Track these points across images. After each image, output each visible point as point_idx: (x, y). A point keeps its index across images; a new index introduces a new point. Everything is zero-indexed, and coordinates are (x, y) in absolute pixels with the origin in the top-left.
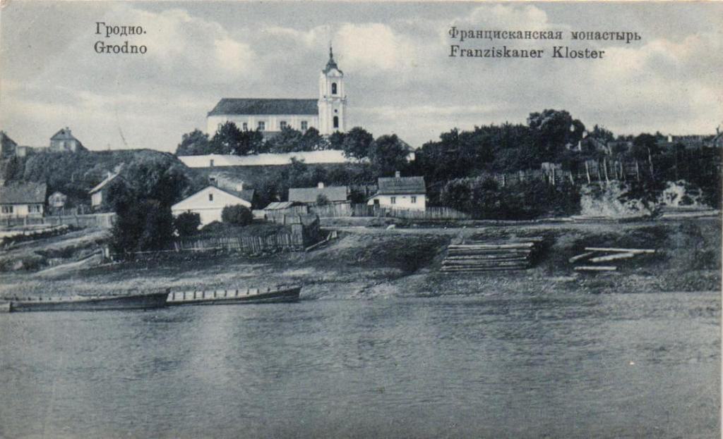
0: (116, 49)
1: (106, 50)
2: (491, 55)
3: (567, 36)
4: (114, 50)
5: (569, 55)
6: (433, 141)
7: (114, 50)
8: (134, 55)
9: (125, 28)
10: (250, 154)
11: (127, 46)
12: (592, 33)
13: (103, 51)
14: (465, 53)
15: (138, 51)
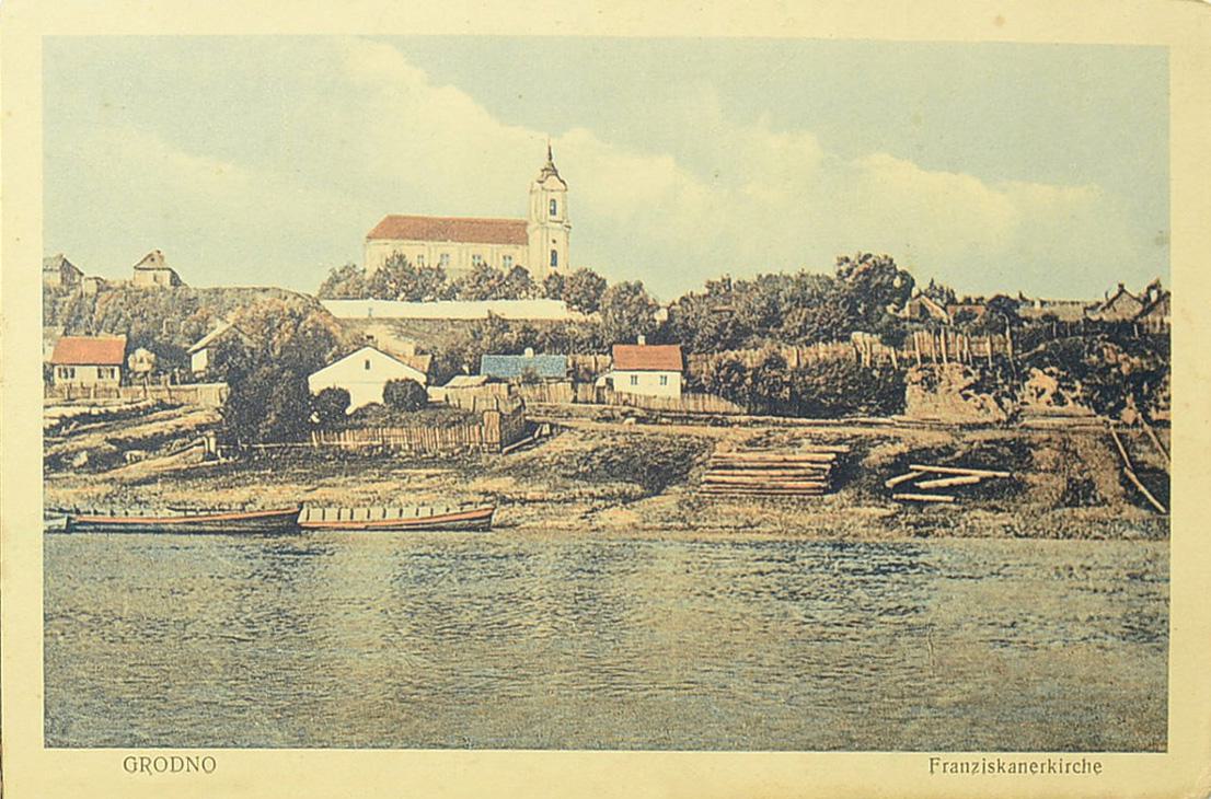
14: (948, 767)
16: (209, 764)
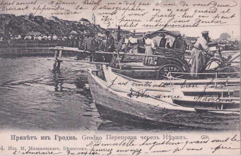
0: (90, 138)
1: (86, 138)
2: (44, 137)
3: (52, 137)
4: (89, 138)
5: (111, 138)
6: (13, 14)
7: (89, 138)
8: (21, 136)
9: (67, 137)
10: (214, 68)
11: (95, 137)
12: (71, 137)
13: (85, 139)
15: (99, 139)
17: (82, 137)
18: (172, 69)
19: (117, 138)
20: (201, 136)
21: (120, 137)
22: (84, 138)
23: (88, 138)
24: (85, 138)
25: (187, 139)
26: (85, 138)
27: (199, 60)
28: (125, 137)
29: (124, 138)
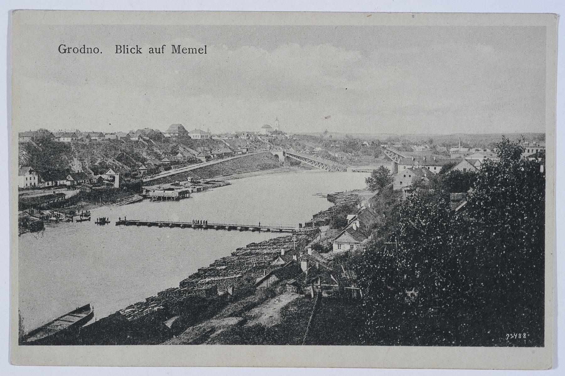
0: (76, 50)
11: (84, 48)
13: (65, 52)
16: (96, 51)
17: (61, 45)
18: (59, 140)
19: (78, 52)
20: (58, 49)
21: (203, 50)
22: (62, 51)
23: (71, 50)
24: (65, 50)
25: (101, 53)
26: (65, 50)
27: (127, 308)
28: (84, 53)
29: (86, 51)
